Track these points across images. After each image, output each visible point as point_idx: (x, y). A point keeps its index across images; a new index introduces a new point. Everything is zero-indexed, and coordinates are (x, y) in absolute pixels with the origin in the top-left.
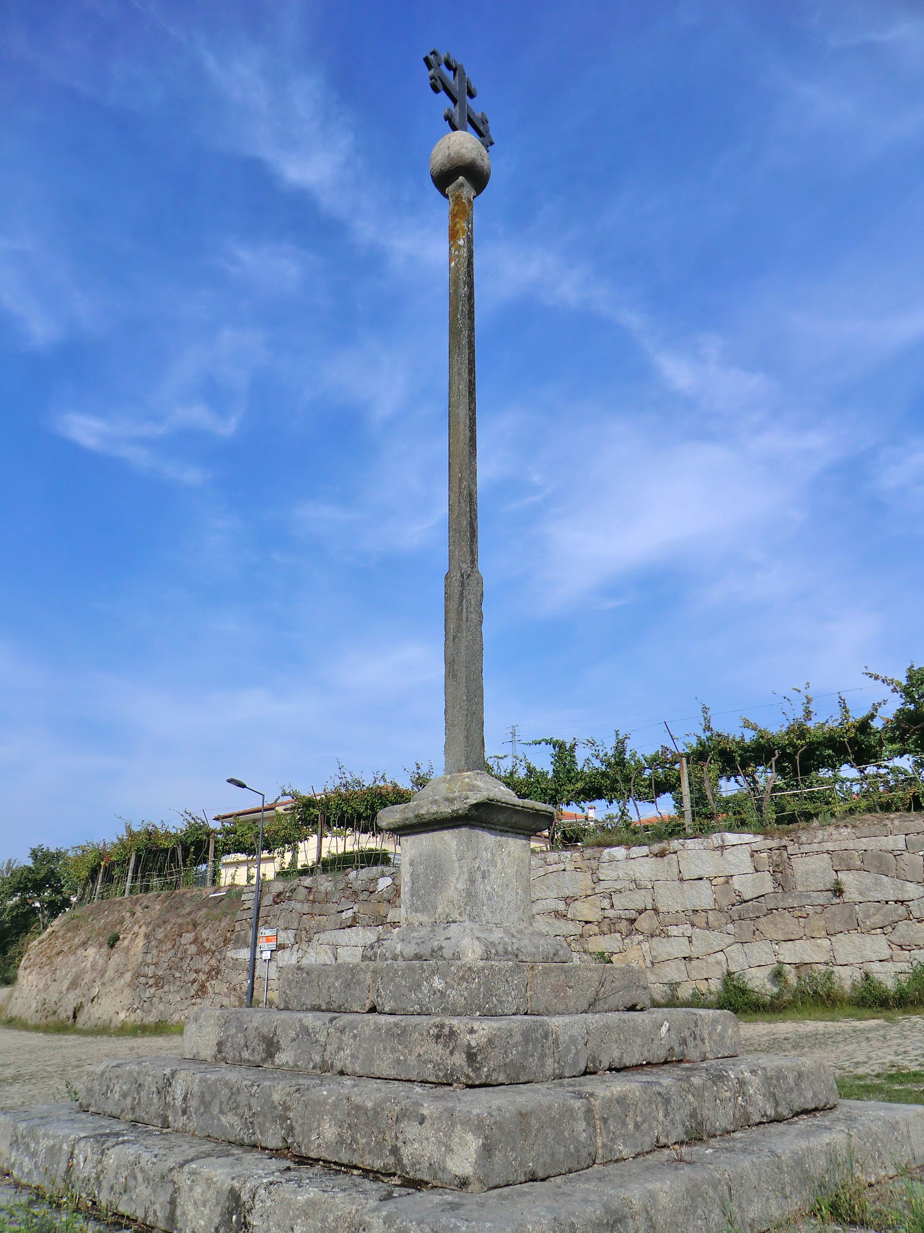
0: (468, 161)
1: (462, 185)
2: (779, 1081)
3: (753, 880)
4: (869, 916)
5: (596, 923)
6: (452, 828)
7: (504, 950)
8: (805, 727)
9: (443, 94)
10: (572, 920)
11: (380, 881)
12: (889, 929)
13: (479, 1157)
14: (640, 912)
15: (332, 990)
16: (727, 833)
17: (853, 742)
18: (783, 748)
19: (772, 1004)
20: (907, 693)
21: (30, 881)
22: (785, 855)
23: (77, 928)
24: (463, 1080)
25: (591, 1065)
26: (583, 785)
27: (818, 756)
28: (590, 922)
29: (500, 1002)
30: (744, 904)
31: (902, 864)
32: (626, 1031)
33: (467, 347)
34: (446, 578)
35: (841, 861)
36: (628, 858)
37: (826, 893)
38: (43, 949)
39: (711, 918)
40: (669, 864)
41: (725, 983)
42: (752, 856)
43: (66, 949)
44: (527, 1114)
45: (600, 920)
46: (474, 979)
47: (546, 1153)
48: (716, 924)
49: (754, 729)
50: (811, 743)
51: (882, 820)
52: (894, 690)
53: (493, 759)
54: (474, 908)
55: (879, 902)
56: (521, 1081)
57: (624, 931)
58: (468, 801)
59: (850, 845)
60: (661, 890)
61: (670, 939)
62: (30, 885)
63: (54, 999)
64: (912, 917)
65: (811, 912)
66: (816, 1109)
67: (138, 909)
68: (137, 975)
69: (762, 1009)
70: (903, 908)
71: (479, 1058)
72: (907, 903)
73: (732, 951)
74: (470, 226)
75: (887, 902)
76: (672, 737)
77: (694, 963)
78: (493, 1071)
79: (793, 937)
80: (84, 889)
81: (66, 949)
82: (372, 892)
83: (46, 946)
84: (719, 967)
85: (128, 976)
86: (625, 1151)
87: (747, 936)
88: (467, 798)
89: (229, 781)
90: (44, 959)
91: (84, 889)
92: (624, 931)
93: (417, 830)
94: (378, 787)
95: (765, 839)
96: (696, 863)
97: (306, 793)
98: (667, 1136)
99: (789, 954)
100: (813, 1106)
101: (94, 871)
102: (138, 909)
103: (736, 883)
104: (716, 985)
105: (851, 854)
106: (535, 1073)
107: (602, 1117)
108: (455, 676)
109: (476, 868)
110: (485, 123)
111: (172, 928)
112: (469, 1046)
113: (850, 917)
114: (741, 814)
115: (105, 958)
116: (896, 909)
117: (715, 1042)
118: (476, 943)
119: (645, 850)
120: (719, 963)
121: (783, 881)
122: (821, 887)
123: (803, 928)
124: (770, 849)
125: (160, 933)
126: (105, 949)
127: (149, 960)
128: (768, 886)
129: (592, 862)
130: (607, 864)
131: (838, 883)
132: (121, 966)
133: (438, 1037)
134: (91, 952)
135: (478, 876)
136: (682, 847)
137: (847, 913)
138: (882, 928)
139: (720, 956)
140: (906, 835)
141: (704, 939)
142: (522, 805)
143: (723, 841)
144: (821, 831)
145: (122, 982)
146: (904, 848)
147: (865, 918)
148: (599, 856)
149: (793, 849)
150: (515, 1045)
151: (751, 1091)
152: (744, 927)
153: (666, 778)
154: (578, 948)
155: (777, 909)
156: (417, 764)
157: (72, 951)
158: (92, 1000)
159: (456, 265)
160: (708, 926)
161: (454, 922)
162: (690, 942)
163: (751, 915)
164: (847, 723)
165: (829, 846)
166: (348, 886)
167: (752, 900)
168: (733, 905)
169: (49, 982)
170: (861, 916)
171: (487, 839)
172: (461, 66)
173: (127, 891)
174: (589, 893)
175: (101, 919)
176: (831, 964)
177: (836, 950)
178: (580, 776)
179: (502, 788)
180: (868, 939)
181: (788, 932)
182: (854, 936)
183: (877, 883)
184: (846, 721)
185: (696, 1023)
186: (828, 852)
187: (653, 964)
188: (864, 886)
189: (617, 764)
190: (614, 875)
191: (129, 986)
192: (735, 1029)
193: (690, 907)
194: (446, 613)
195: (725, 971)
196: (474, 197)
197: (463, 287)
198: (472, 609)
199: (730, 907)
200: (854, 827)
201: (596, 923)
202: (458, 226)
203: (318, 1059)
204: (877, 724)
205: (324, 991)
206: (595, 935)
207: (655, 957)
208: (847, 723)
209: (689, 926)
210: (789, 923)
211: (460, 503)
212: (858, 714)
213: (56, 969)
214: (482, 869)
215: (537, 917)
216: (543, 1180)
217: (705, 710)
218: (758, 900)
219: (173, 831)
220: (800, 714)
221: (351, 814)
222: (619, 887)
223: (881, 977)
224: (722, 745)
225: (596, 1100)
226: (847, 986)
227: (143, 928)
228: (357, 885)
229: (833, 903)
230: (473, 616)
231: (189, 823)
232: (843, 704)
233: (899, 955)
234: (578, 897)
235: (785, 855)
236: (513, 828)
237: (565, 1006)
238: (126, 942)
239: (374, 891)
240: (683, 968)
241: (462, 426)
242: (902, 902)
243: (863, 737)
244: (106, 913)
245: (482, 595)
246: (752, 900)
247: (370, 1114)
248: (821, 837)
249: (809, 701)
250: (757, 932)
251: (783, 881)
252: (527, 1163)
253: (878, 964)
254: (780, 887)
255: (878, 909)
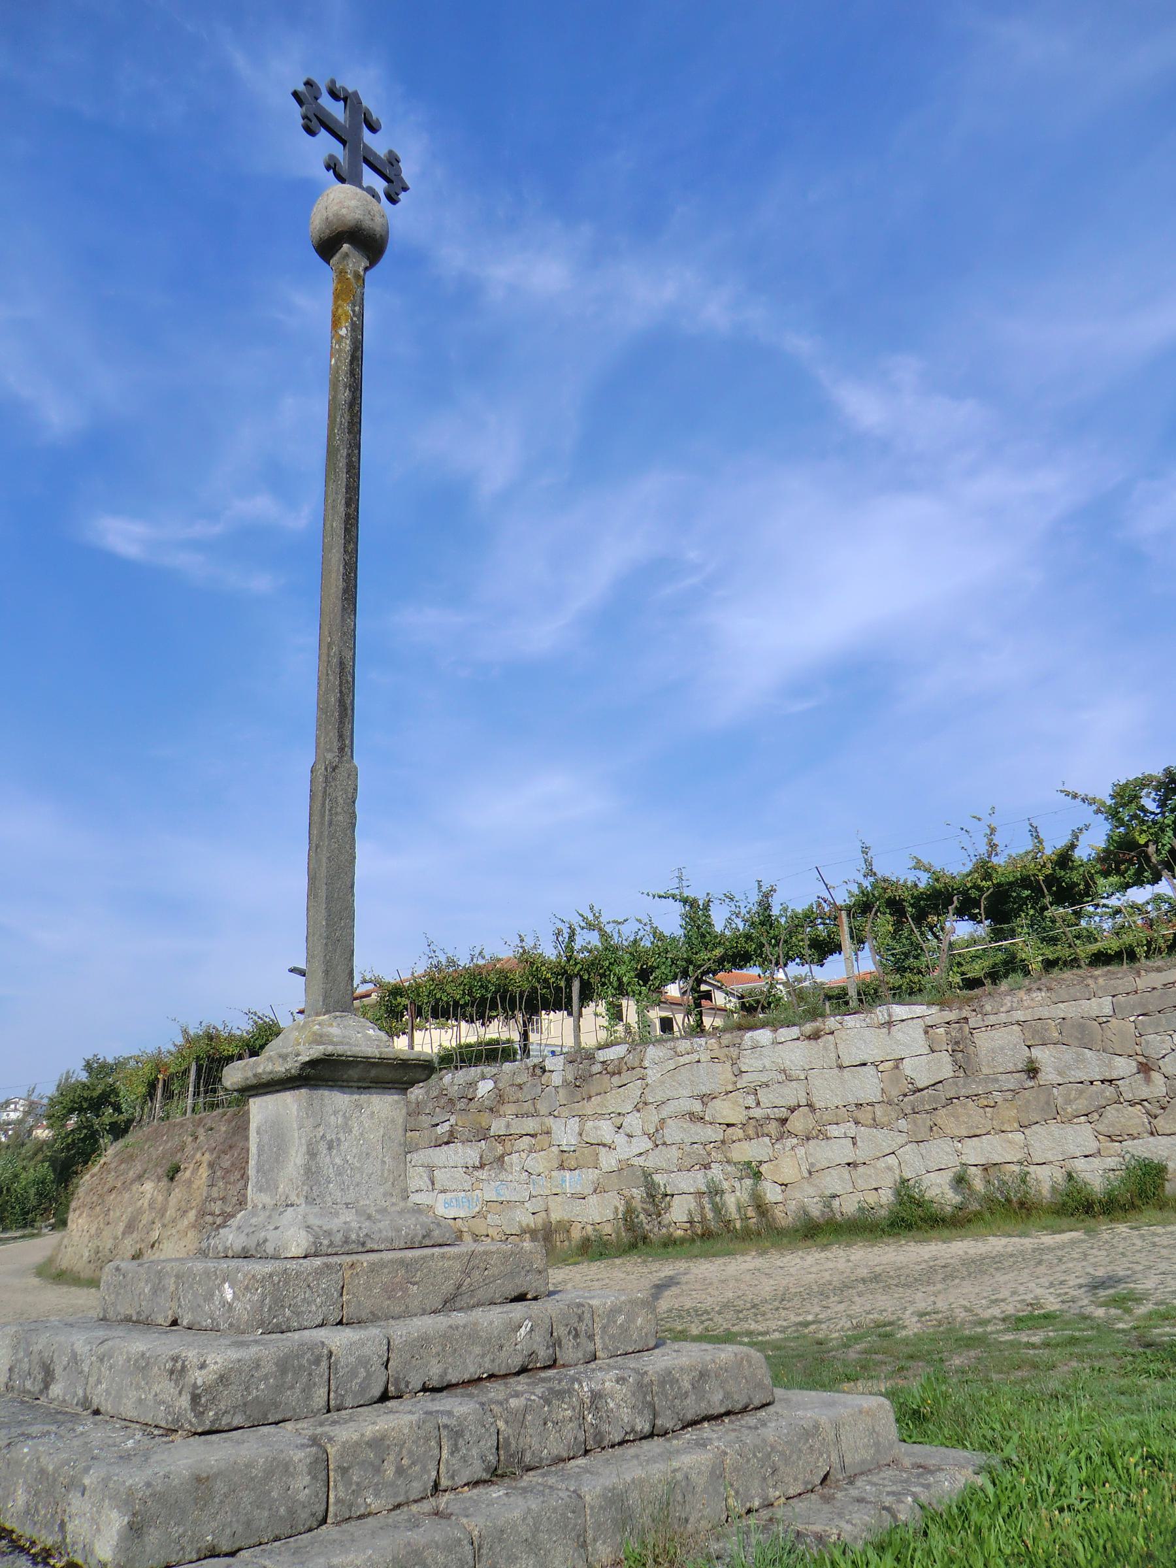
0: (352, 223)
1: (346, 255)
2: (664, 1387)
3: (929, 1062)
4: (1071, 1101)
5: (740, 1126)
6: (293, 1088)
7: (344, 1239)
8: (989, 865)
9: (323, 133)
10: (711, 1124)
11: (480, 1084)
12: (1096, 1116)
13: (123, 1538)
14: (792, 1110)
15: (142, 1297)
16: (894, 1006)
17: (1051, 880)
18: (965, 893)
19: (953, 1216)
20: (1113, 814)
21: (86, 1099)
22: (966, 1029)
23: (132, 1158)
24: (187, 1426)
25: (393, 1388)
26: (723, 951)
27: (1014, 898)
28: (733, 1125)
29: (298, 1314)
30: (918, 1094)
31: (1109, 1034)
32: (456, 1339)
33: (345, 470)
34: (312, 772)
35: (1035, 1033)
36: (776, 1043)
37: (1018, 1074)
38: (95, 1185)
39: (878, 1113)
40: (825, 1048)
41: (898, 1193)
42: (926, 1033)
43: (119, 1185)
44: (208, 1478)
45: (744, 1122)
46: (257, 1290)
47: (238, 1521)
48: (885, 1120)
49: (927, 870)
50: (999, 885)
51: (1084, 979)
52: (1098, 811)
53: (612, 925)
54: (314, 1188)
55: (1082, 1083)
56: (270, 1421)
57: (774, 1133)
58: (300, 1058)
59: (1045, 1013)
60: (816, 1082)
61: (830, 1142)
62: (85, 1105)
63: (108, 1247)
64: (1122, 1100)
65: (999, 1100)
66: (728, 1413)
67: (201, 1131)
68: (202, 1213)
69: (941, 1223)
70: (1111, 1089)
71: (203, 1400)
72: (1117, 1082)
73: (905, 1153)
74: (357, 308)
75: (1092, 1083)
76: (826, 885)
77: (861, 1169)
78: (223, 1414)
79: (978, 1132)
80: (142, 1109)
81: (119, 1185)
82: (471, 1100)
83: (97, 1182)
84: (890, 1173)
85: (192, 1215)
86: (373, 1502)
87: (923, 1134)
88: (298, 1055)
89: (291, 971)
90: (95, 1198)
91: (142, 1109)
92: (774, 1133)
93: (261, 1091)
94: (477, 965)
95: (941, 1010)
96: (858, 1045)
97: (391, 979)
98: (452, 1477)
99: (975, 1153)
100: (723, 1410)
101: (152, 1086)
102: (201, 1131)
103: (907, 1067)
104: (886, 1197)
105: (1047, 1024)
106: (294, 1409)
107: (339, 1467)
108: (316, 896)
109: (318, 1138)
110: (395, 163)
111: (239, 1155)
112: (195, 1386)
113: (1048, 1103)
114: (962, 965)
115: (165, 1193)
116: (1103, 1091)
117: (612, 1337)
118: (303, 1233)
119: (795, 1032)
120: (890, 1168)
121: (964, 1065)
122: (1011, 1068)
123: (992, 1120)
124: (948, 1023)
125: (226, 1162)
126: (164, 1182)
127: (215, 1195)
128: (946, 1069)
129: (732, 1049)
130: (749, 1051)
131: (1031, 1061)
132: (183, 1203)
133: (172, 1372)
134: (148, 1188)
135: (323, 1147)
136: (840, 1026)
137: (1043, 1098)
138: (1087, 1115)
139: (891, 1160)
140: (1114, 996)
141: (871, 1140)
142: (378, 1056)
143: (890, 1015)
144: (1009, 998)
145: (186, 1222)
146: (1111, 1013)
147: (1066, 1104)
148: (739, 1041)
149: (977, 1022)
150: (265, 1378)
151: (612, 1405)
152: (920, 1121)
153: (829, 936)
154: (720, 1157)
155: (958, 1098)
156: (520, 936)
157: (126, 1186)
158: (153, 1246)
159: (336, 363)
160: (876, 1124)
161: (292, 1205)
162: (854, 1144)
163: (927, 1107)
164: (1041, 857)
165: (1019, 1015)
166: (442, 1093)
167: (927, 1088)
168: (905, 1095)
169: (102, 1226)
170: (1060, 1101)
171: (337, 1100)
172: (356, 94)
173: (189, 1111)
174: (730, 1088)
175: (160, 1146)
176: (1026, 1163)
177: (1032, 1145)
178: (718, 941)
179: (371, 1032)
180: (1068, 1129)
181: (972, 1126)
182: (1053, 1126)
183: (1080, 1060)
184: (1040, 854)
185: (580, 1317)
186: (1018, 1023)
187: (810, 1173)
188: (1063, 1064)
189: (762, 924)
190: (758, 1065)
191: (194, 1226)
192: (650, 1316)
193: (853, 1100)
194: (310, 815)
195: (898, 1178)
196: (366, 269)
197: (342, 392)
198: (339, 810)
199: (901, 1098)
200: (1049, 989)
201: (740, 1126)
202: (340, 311)
203: (80, 1393)
204: (1082, 853)
205: (136, 1298)
206: (740, 1140)
207: (812, 1165)
208: (1041, 857)
209: (852, 1124)
210: (973, 1117)
211: (328, 675)
212: (1054, 844)
213: (109, 1210)
214: (328, 1138)
215: (669, 1120)
216: (232, 1554)
217: (865, 850)
218: (935, 1087)
219: (238, 1033)
220: (983, 849)
221: (448, 1003)
222: (764, 1080)
223: (1088, 1177)
224: (889, 894)
225: (332, 1446)
226: (1046, 1190)
227: (207, 1155)
228: (454, 1091)
229: (1026, 1086)
230: (340, 818)
231: (256, 1023)
232: (1035, 833)
233: (1107, 1148)
234: (717, 1094)
235: (966, 1029)
236: (376, 1083)
237: (403, 1307)
238: (188, 1174)
239: (473, 1098)
240: (847, 1176)
241: (334, 575)
242: (1111, 1081)
243: (1063, 873)
244: (165, 1138)
245: (356, 789)
246: (927, 1088)
247: (51, 1478)
248: (1009, 1005)
249: (993, 831)
250: (935, 1128)
251: (964, 1065)
252: (203, 1536)
253: (1083, 1160)
254: (962, 1070)
255: (1081, 1092)
